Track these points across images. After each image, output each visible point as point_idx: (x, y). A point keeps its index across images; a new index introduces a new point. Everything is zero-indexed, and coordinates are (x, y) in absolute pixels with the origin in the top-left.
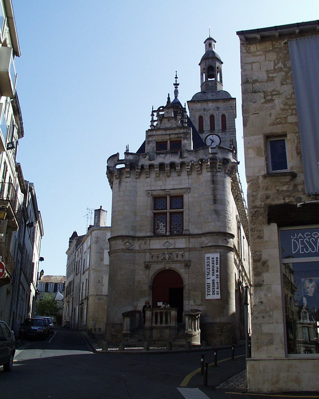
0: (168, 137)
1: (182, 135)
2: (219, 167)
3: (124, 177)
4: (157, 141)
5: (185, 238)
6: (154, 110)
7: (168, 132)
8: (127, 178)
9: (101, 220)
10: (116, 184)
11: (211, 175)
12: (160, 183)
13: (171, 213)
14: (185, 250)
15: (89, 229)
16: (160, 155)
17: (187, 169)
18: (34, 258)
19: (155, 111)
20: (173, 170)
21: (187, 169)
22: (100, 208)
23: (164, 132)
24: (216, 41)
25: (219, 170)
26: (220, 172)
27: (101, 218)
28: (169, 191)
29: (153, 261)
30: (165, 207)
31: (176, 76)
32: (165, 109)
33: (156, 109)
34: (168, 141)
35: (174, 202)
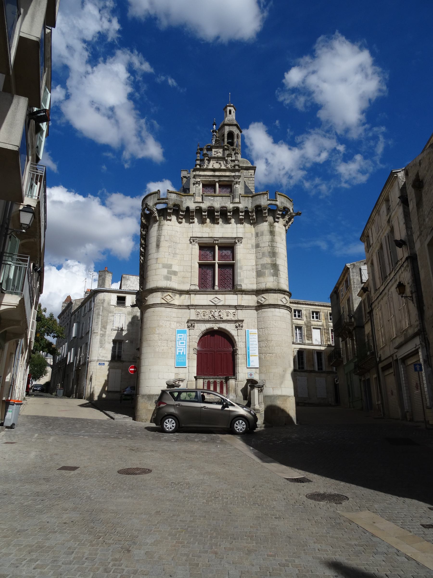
7: (217, 173)
17: (241, 215)
21: (241, 215)
29: (198, 319)
34: (217, 185)
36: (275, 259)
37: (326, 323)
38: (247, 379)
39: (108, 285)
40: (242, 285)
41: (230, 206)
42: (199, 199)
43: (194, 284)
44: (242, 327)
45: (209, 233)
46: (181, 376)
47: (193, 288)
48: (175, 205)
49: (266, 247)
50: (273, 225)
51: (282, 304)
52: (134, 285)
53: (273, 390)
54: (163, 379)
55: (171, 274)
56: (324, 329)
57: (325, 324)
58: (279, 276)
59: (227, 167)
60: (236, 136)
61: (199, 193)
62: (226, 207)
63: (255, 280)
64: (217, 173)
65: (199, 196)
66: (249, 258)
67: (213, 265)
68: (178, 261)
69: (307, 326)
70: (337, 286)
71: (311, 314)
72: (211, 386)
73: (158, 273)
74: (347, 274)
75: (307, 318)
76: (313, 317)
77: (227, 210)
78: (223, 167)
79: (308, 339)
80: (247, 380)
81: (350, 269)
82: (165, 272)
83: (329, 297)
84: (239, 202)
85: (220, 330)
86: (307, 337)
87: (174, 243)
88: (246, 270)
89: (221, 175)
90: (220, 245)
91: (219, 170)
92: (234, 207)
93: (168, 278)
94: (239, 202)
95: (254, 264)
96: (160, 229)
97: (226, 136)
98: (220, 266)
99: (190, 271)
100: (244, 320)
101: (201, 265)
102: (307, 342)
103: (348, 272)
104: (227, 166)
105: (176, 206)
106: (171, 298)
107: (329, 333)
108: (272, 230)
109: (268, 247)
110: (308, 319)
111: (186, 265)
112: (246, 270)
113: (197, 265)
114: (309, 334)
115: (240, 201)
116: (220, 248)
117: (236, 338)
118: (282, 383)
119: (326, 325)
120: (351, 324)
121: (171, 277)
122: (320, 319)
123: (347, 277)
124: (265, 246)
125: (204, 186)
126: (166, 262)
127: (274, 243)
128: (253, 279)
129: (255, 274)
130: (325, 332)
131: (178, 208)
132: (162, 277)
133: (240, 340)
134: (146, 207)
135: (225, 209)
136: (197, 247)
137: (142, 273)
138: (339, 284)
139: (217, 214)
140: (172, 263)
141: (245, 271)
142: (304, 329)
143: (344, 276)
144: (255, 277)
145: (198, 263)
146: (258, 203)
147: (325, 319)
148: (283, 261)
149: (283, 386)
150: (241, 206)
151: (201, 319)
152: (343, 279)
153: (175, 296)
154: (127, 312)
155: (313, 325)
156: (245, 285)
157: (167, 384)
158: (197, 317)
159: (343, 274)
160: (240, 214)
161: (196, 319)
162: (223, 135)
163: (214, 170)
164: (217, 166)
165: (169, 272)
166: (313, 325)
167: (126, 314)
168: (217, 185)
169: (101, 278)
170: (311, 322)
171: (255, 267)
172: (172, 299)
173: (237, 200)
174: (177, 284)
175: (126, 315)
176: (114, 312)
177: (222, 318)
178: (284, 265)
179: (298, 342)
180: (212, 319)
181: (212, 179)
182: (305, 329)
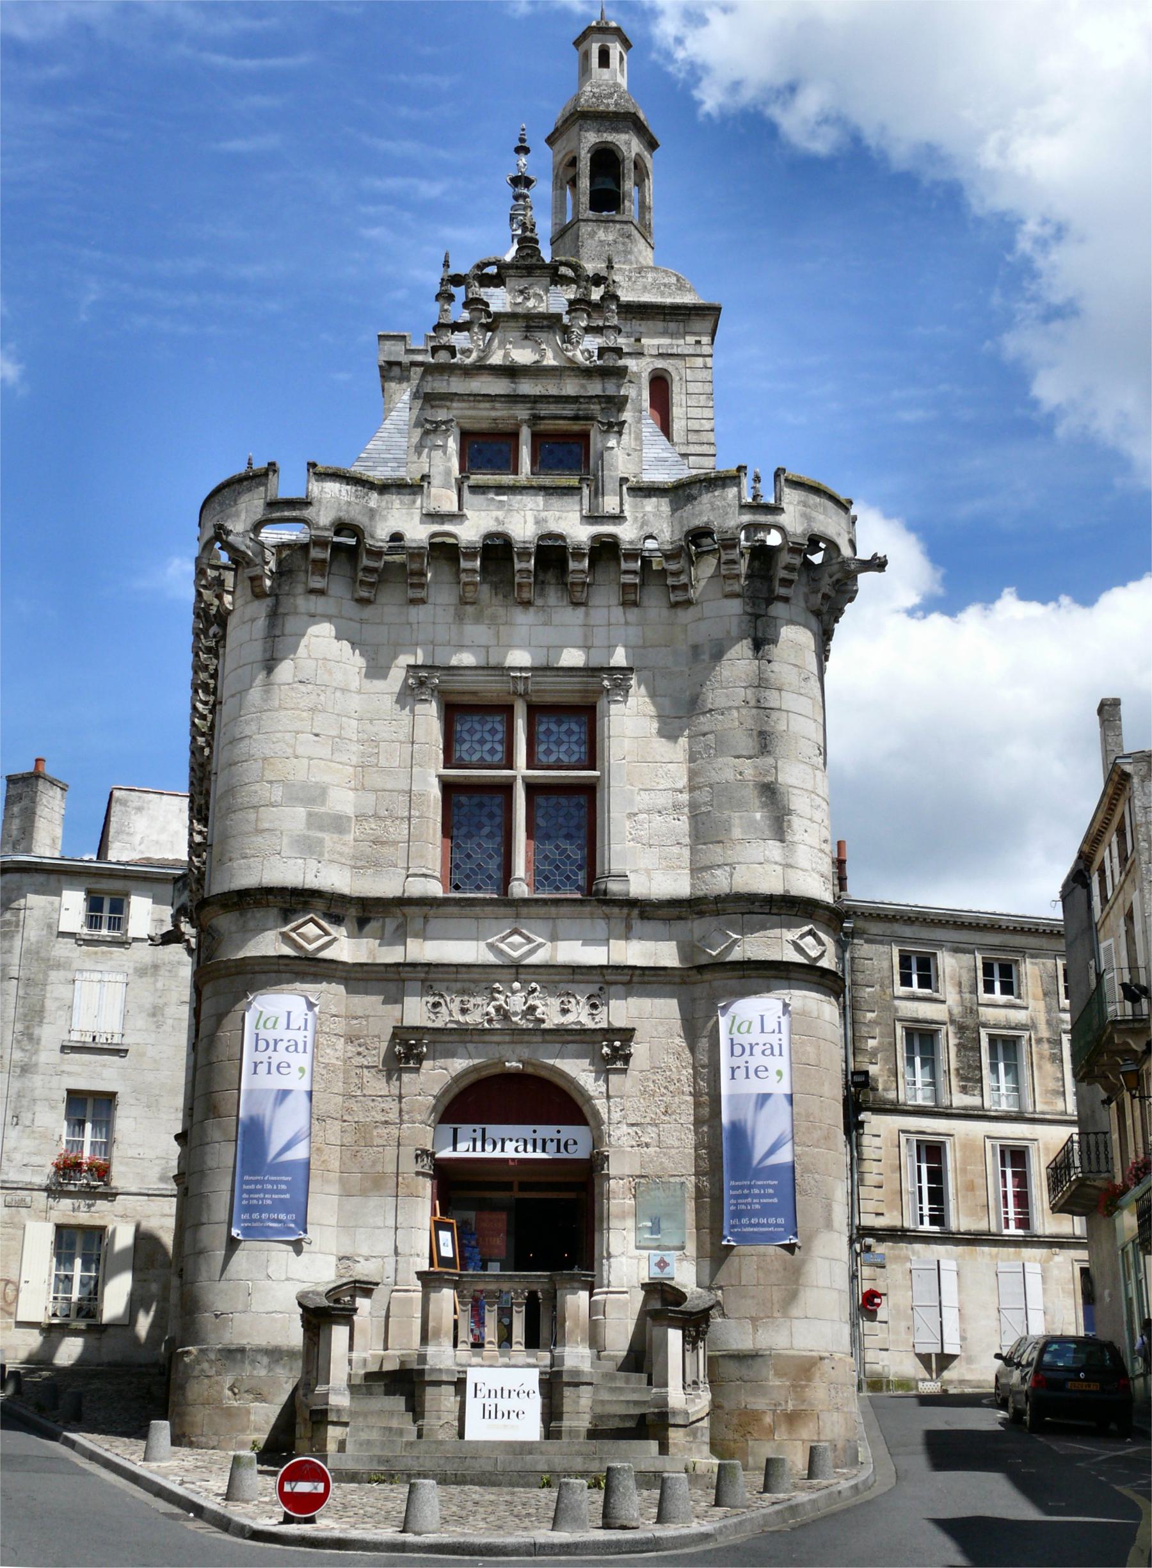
0: (522, 413)
1: (595, 408)
2: (783, 574)
3: (300, 589)
4: (468, 425)
5: (607, 917)
6: (452, 271)
7: (527, 387)
8: (313, 597)
9: (36, 824)
10: (253, 620)
11: (746, 613)
12: (477, 632)
13: (533, 789)
14: (609, 978)
15: (1100, 711)
16: (491, 496)
17: (627, 572)
18: (1145, 932)
19: (457, 280)
20: (550, 577)
21: (627, 572)
22: (31, 769)
23: (499, 386)
24: (632, 41)
25: (782, 591)
26: (786, 600)
27: (37, 818)
28: (526, 678)
29: (439, 1024)
30: (497, 757)
31: (522, 140)
32: (512, 272)
33: (463, 267)
34: (525, 434)
35: (548, 729)
36: (770, 760)
37: (1049, 1011)
38: (647, 1281)
39: (48, 841)
40: (631, 877)
41: (580, 533)
42: (447, 501)
43: (424, 871)
44: (627, 1058)
45: (488, 647)
46: (364, 1270)
47: (419, 888)
48: (341, 527)
49: (735, 713)
50: (765, 615)
51: (799, 959)
52: (164, 837)
53: (755, 1330)
54: (288, 1279)
55: (321, 828)
56: (1039, 1041)
57: (1042, 1019)
58: (788, 838)
59: (570, 360)
60: (629, 166)
61: (448, 472)
62: (561, 537)
63: (686, 852)
64: (527, 387)
65: (446, 486)
66: (658, 758)
67: (505, 789)
68: (351, 770)
69: (961, 1029)
70: (1086, 849)
71: (980, 973)
72: (487, 1315)
73: (266, 825)
74: (1122, 801)
75: (960, 992)
76: (989, 988)
77: (565, 548)
78: (550, 360)
79: (964, 1090)
80: (644, 1286)
81: (1136, 780)
82: (293, 819)
83: (1057, 897)
84: (617, 511)
85: (530, 1070)
86: (963, 1078)
87: (338, 694)
88: (649, 812)
89: (544, 393)
90: (535, 699)
91: (535, 371)
92: (595, 538)
93: (308, 847)
94: (617, 511)
95: (683, 782)
96: (278, 633)
97: (585, 165)
98: (533, 789)
99: (406, 814)
100: (634, 1029)
101: (449, 788)
102: (960, 1100)
103: (1127, 794)
104: (570, 354)
105: (345, 532)
106: (321, 933)
107: (1062, 1061)
108: (760, 635)
109: (744, 711)
110: (967, 996)
111: (389, 786)
112: (649, 812)
113: (435, 792)
114: (970, 1066)
115: (622, 511)
116: (534, 711)
117: (600, 1104)
118: (792, 1297)
119: (1049, 1023)
120: (1137, 1025)
121: (321, 842)
122: (1019, 997)
123: (1123, 816)
124: (731, 704)
125: (466, 437)
126: (301, 776)
127: (768, 693)
128: (676, 850)
129: (683, 825)
130: (1041, 1057)
131: (352, 541)
132: (285, 840)
133: (616, 1116)
134: (217, 537)
135: (560, 543)
136: (429, 716)
137: (200, 800)
138: (1093, 840)
139: (524, 565)
140: (326, 778)
141: (641, 817)
142: (949, 1044)
143: (1111, 808)
144: (687, 840)
145: (439, 777)
146: (699, 522)
147: (1046, 994)
148: (809, 770)
149: (795, 1312)
150: (626, 533)
151: (450, 1026)
152: (1106, 823)
153: (347, 909)
154: (132, 965)
155: (985, 1026)
156: (643, 878)
157: (300, 1304)
158: (433, 1017)
159: (1106, 800)
160: (624, 566)
161: (430, 1024)
162: (573, 162)
163: (511, 371)
164: (523, 356)
165: (314, 821)
166: (985, 1026)
167: (131, 971)
168: (525, 434)
169: (16, 809)
170: (982, 1009)
171: (685, 797)
172: (326, 939)
173: (610, 504)
174: (347, 873)
175: (130, 978)
176: (75, 966)
177: (543, 1021)
178: (809, 787)
179: (920, 1101)
180: (498, 1026)
181: (500, 412)
182: (953, 1041)
